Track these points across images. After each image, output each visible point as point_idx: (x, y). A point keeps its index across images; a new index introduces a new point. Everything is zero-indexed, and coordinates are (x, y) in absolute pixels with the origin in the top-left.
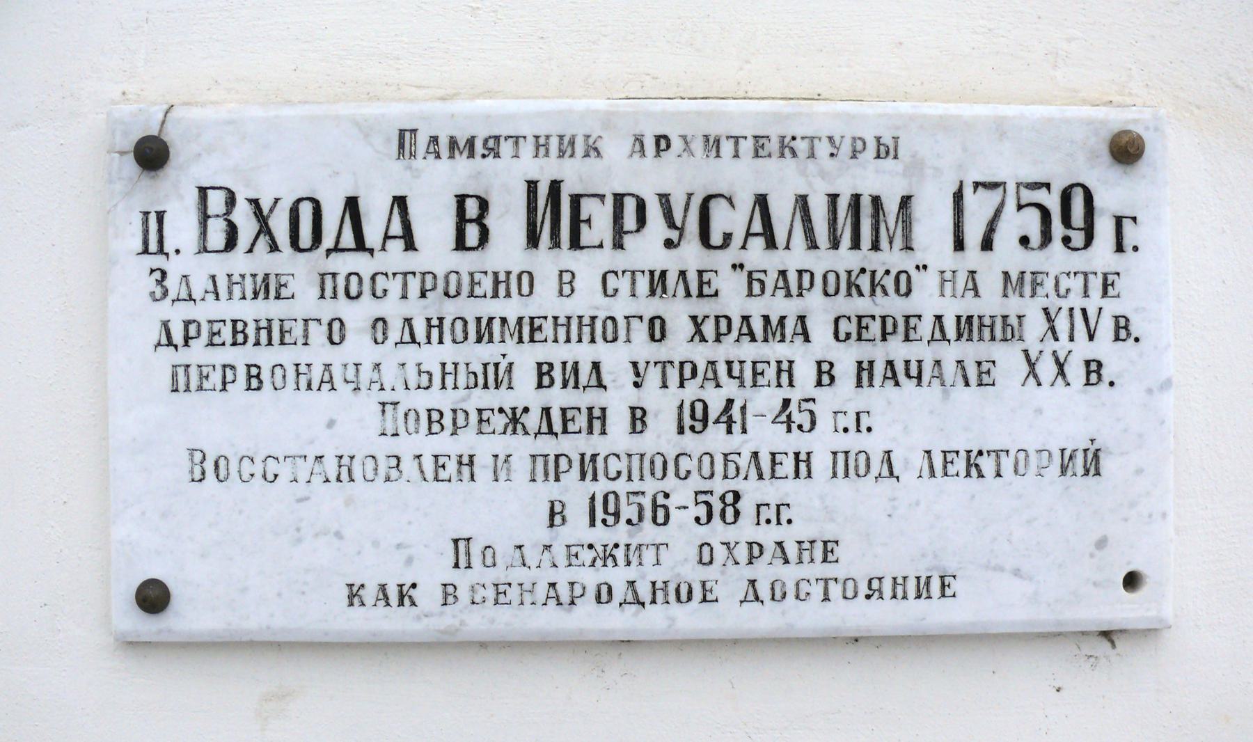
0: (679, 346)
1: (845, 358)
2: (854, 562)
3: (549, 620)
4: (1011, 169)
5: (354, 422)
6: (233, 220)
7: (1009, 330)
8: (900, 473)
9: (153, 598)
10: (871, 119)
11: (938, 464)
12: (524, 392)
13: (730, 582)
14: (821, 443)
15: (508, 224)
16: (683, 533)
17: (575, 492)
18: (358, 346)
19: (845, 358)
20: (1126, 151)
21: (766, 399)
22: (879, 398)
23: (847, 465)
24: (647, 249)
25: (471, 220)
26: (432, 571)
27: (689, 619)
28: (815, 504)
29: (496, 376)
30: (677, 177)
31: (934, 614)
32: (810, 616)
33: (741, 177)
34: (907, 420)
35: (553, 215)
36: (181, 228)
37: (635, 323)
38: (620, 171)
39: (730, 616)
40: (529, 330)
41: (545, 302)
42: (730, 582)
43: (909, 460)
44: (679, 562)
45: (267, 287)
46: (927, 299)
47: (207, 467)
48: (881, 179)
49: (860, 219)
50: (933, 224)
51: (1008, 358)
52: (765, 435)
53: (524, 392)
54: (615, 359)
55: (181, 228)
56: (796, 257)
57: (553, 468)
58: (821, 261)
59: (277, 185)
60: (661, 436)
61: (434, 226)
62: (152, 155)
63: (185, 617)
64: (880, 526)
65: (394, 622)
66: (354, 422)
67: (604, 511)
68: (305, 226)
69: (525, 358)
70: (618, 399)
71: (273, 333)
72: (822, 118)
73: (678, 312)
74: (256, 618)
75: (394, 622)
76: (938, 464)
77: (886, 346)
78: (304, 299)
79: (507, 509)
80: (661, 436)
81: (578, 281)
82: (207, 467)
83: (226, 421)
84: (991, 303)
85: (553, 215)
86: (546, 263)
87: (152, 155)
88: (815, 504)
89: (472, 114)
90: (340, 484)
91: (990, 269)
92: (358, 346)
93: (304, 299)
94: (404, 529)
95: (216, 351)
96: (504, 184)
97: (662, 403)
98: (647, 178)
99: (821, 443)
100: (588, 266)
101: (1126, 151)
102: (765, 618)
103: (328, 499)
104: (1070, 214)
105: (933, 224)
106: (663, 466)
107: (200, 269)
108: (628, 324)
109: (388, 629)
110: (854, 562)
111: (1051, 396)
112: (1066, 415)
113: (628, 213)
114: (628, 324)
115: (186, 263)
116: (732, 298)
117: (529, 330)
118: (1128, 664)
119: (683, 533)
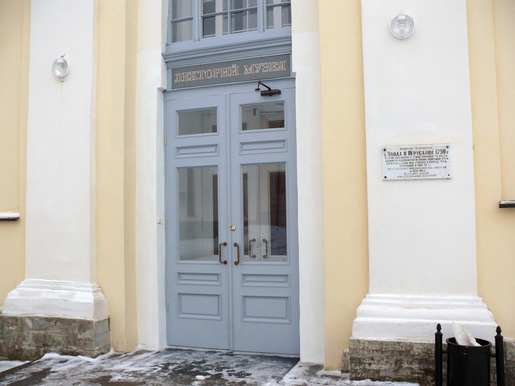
0: (418, 161)
1: (429, 161)
2: (430, 174)
3: (411, 178)
4: (440, 149)
5: (398, 166)
6: (390, 154)
7: (440, 159)
8: (433, 169)
9: (385, 177)
10: (430, 146)
11: (435, 168)
12: (409, 164)
13: (422, 175)
14: (427, 167)
15: (407, 154)
16: (419, 172)
17: (412, 170)
18: (398, 161)
19: (429, 161)
20: (447, 147)
21: (418, 161)
22: (431, 164)
23: (429, 168)
24: (416, 155)
25: (405, 153)
26: (403, 175)
27: (419, 178)
28: (427, 170)
29: (407, 163)
30: (418, 150)
31: (435, 177)
32: (427, 177)
33: (422, 150)
34: (433, 165)
35: (410, 153)
36: (387, 154)
37: (197, 38)
38: (414, 150)
39: (422, 178)
40: (409, 160)
41: (410, 158)
42: (422, 175)
43: (433, 168)
44: (419, 174)
45: (392, 158)
46: (434, 157)
47: (389, 169)
48: (431, 150)
49: (430, 152)
50: (434, 153)
51: (440, 161)
52: (424, 166)
53: (409, 164)
54: (414, 162)
55: (387, 154)
56: (426, 155)
57: (410, 169)
58: (427, 155)
59: (393, 152)
60: (417, 166)
61: (403, 154)
62: (385, 150)
63: (387, 179)
64: (432, 172)
65: (401, 178)
66: (398, 166)
67: (414, 171)
68: (395, 154)
69: (409, 162)
70: (414, 165)
71: (393, 161)
72: (427, 146)
73: (418, 159)
74: (392, 178)
75: (401, 178)
76: (435, 168)
77: (431, 160)
78: (395, 159)
79: (408, 171)
80: (417, 166)
81: (412, 157)
82: (389, 169)
83: (390, 166)
84: (438, 157)
85: (410, 153)
86: (410, 156)
87: (385, 150)
88: (427, 170)
89: (405, 147)
90: (397, 170)
91: (438, 155)
92: (398, 161)
93: (395, 159)
94: (401, 172)
95: (389, 162)
96: (407, 151)
97: (417, 164)
98: (416, 150)
99: (427, 167)
100: (412, 156)
101: (447, 147)
102: (424, 178)
103: (396, 171)
104: (444, 151)
105: (434, 153)
106: (417, 168)
107: (388, 157)
108: (244, 304)
109: (400, 179)
110: (430, 174)
111: (443, 163)
112: (444, 164)
113: (415, 153)
114: (244, 304)
115: (387, 157)
116: (421, 158)
117: (409, 160)
118: (449, 181)
119: (419, 172)
